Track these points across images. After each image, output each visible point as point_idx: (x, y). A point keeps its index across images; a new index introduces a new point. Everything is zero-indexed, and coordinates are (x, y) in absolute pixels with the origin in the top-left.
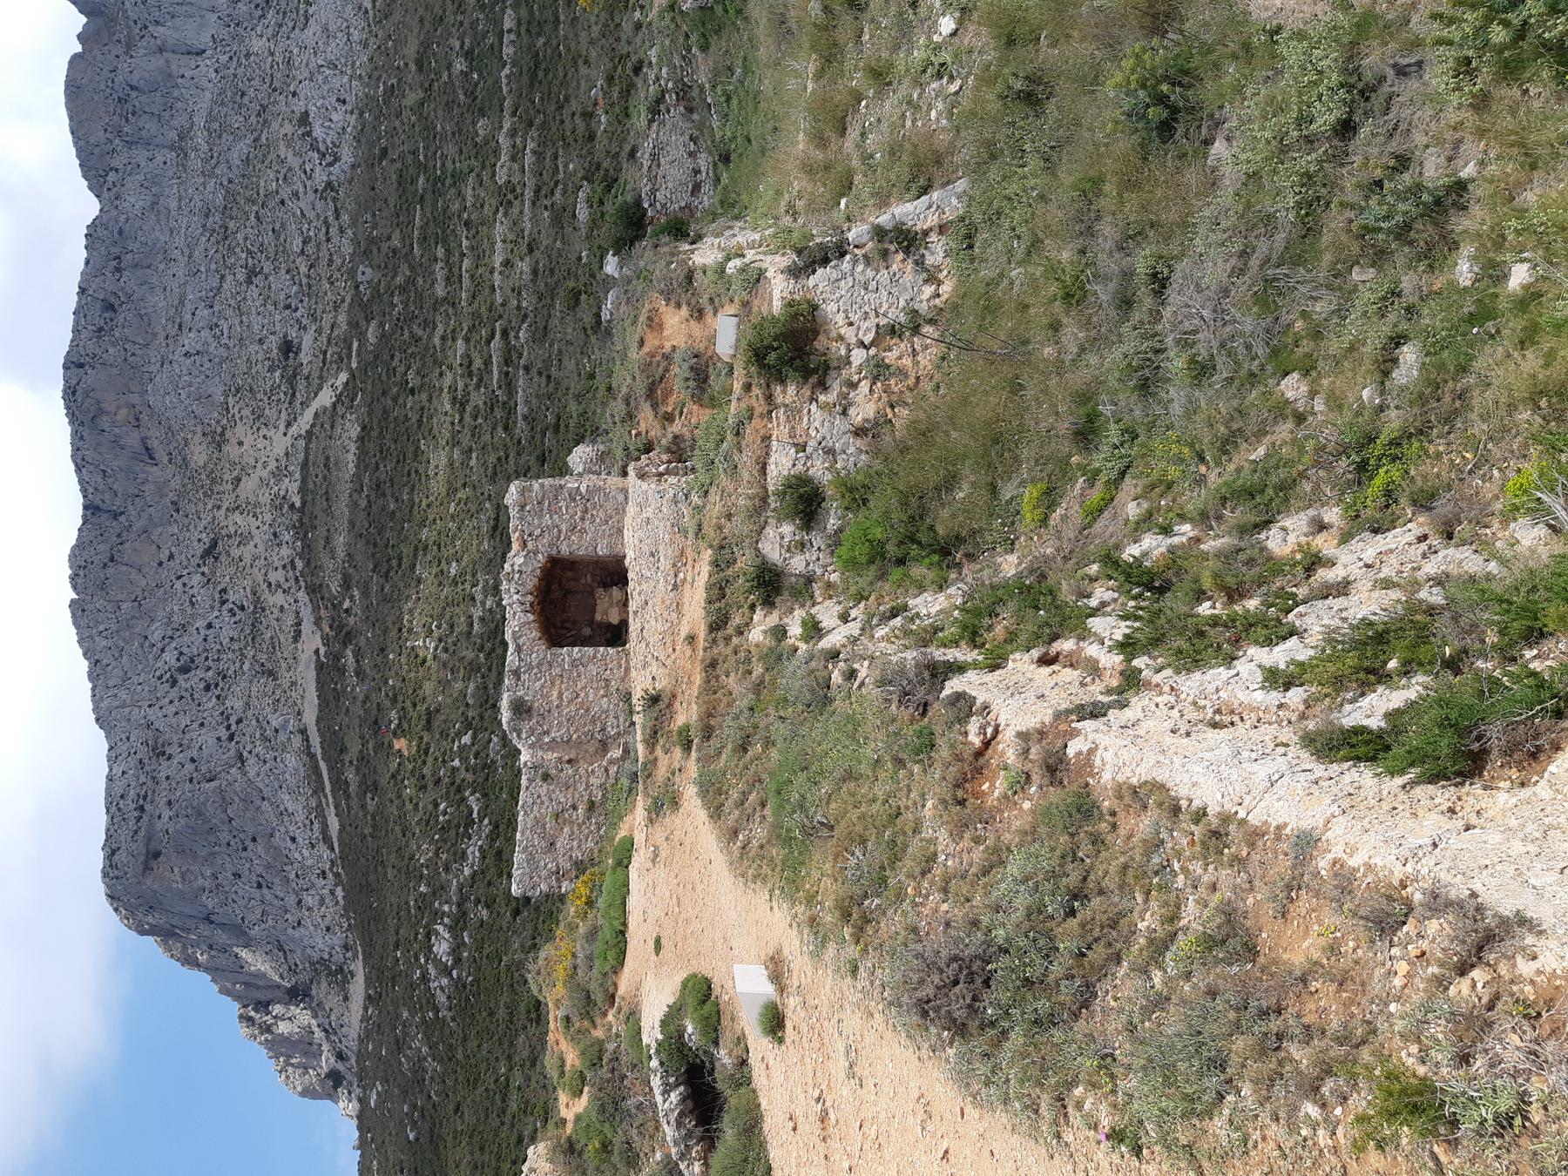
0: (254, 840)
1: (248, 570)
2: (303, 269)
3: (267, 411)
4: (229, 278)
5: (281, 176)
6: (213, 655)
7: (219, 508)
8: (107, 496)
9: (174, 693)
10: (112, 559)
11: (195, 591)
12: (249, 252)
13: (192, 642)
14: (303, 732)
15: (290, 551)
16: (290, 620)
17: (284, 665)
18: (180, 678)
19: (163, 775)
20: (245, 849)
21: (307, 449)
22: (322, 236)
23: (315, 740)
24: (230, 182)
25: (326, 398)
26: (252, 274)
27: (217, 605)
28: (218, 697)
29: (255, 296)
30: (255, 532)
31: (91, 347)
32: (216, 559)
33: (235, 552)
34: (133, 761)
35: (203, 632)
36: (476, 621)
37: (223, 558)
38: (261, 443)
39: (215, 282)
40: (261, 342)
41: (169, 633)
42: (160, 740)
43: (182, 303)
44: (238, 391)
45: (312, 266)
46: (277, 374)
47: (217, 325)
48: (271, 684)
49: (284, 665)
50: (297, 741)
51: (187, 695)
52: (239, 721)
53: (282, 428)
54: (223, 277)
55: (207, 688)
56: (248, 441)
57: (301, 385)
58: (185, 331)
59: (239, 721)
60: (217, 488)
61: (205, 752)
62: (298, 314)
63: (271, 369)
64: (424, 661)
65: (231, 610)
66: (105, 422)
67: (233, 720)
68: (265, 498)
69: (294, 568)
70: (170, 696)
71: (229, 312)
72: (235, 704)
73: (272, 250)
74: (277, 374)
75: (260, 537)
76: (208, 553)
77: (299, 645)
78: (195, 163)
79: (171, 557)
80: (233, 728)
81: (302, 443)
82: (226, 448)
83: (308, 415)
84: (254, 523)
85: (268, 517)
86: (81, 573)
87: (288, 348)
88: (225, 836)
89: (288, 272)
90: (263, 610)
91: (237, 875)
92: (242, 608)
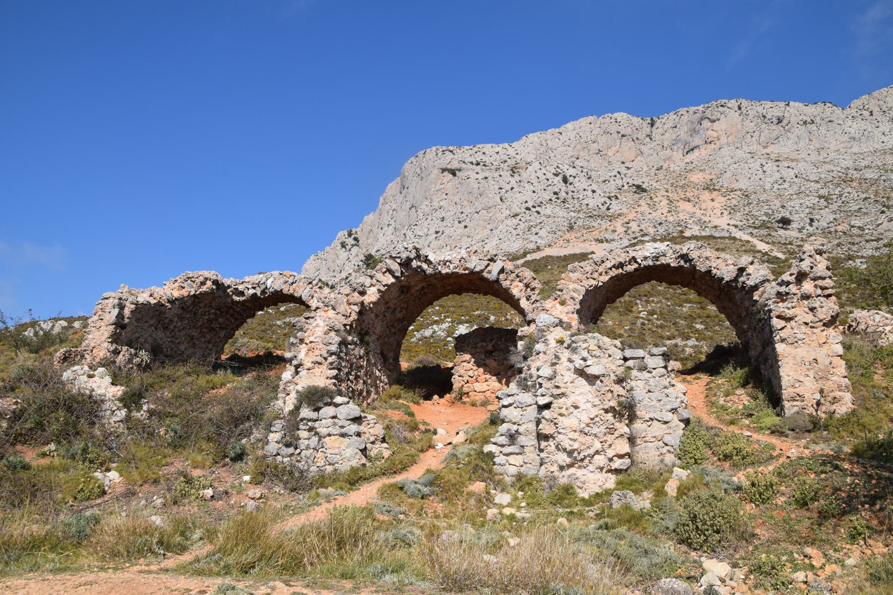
0: (466, 227)
2: (840, 228)
4: (819, 186)
7: (667, 191)
8: (660, 130)
9: (550, 176)
10: (623, 136)
11: (612, 182)
12: (841, 196)
13: (580, 183)
14: (538, 249)
15: (653, 233)
16: (609, 236)
17: (579, 235)
18: (560, 178)
19: (502, 173)
20: (460, 222)
21: (724, 238)
22: (868, 237)
23: (537, 256)
25: (762, 246)
26: (827, 198)
27: (607, 195)
28: (550, 200)
29: (812, 201)
30: (659, 212)
32: (635, 192)
33: (642, 202)
34: (506, 158)
35: (589, 188)
36: (673, 342)
37: (637, 196)
38: (718, 213)
39: (812, 178)
40: (783, 207)
42: (520, 170)
43: (793, 161)
44: (746, 196)
45: (844, 233)
46: (764, 218)
47: (784, 181)
48: (565, 229)
49: (579, 235)
50: (532, 246)
52: (538, 213)
53: (732, 222)
54: (817, 182)
55: (555, 193)
56: (715, 204)
57: (764, 232)
58: (777, 163)
59: (538, 213)
60: (679, 190)
62: (808, 227)
63: (767, 214)
64: (631, 311)
66: (706, 124)
67: (538, 209)
68: (682, 216)
69: (643, 236)
71: (795, 188)
73: (846, 208)
74: (764, 218)
75: (657, 216)
76: (638, 187)
77: (594, 242)
79: (628, 168)
80: (534, 210)
81: (727, 235)
84: (665, 211)
85: (671, 219)
87: (785, 222)
88: (467, 210)
89: (835, 219)
91: (443, 219)
92: (608, 209)
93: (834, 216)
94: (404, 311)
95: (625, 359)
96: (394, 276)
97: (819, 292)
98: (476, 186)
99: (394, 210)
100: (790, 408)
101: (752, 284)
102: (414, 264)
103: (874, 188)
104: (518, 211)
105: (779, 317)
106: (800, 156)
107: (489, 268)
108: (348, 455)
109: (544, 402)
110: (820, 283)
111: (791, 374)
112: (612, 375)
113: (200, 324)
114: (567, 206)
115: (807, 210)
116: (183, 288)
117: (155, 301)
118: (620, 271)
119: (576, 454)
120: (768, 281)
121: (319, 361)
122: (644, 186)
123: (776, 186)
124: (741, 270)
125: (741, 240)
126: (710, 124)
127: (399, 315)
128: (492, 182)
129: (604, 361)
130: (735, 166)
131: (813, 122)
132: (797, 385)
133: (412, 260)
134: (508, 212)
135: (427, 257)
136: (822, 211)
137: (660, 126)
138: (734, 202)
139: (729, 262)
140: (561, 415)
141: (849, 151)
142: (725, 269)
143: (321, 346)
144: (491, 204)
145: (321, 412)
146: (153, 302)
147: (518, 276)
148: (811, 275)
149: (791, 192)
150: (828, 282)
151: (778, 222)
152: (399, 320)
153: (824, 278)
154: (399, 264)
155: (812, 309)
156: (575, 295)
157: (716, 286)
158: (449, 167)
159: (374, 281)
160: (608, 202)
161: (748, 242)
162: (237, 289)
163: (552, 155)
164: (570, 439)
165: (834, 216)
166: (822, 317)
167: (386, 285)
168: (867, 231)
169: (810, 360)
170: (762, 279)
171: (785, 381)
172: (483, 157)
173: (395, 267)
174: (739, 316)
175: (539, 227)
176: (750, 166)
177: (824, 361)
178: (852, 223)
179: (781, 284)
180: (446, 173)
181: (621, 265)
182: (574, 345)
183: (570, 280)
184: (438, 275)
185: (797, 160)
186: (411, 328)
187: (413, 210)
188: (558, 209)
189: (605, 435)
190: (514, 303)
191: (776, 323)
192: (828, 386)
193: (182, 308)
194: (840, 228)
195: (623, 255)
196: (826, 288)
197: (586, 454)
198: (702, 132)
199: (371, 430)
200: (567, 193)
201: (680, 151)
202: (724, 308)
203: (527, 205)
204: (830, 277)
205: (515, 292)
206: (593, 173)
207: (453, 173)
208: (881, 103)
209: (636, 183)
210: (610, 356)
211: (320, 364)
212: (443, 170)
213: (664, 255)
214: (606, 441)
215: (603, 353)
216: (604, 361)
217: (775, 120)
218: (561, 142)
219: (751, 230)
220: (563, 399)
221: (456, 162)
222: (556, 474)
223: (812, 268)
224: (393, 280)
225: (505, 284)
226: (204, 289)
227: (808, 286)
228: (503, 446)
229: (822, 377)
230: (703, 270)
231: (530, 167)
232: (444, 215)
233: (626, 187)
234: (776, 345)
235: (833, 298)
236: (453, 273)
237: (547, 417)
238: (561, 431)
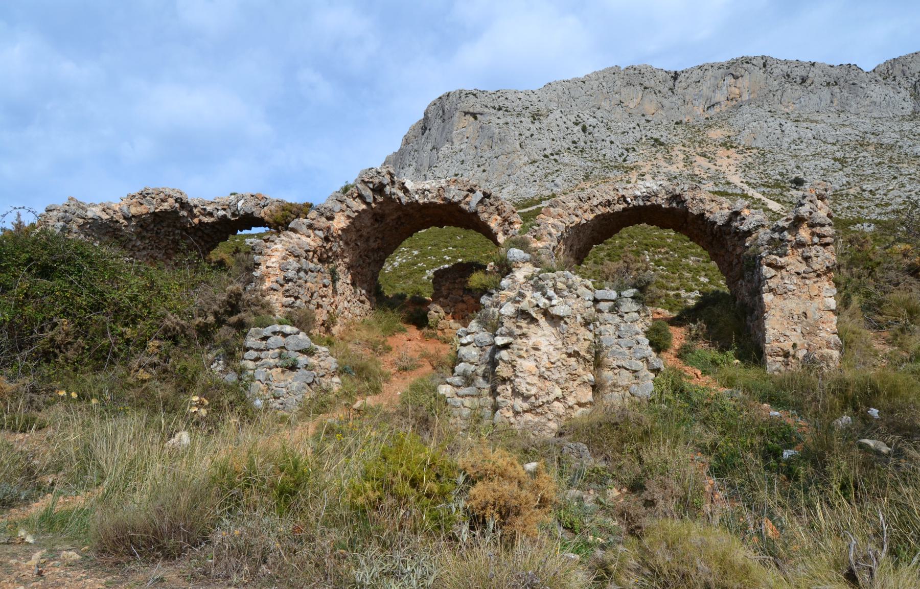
1: (650, 163)
2: (852, 191)
3: (753, 172)
4: (835, 148)
5: (912, 176)
6: (594, 145)
9: (570, 124)
10: (645, 88)
11: (631, 134)
12: (856, 159)
13: (600, 133)
18: (579, 128)
19: (523, 119)
20: (479, 166)
24: (900, 147)
26: (843, 161)
27: (625, 146)
28: (569, 149)
29: (828, 163)
31: (777, 72)
33: (659, 155)
34: (527, 104)
35: (608, 139)
37: (654, 149)
39: (830, 140)
40: (798, 167)
41: (605, 121)
42: (541, 118)
43: (812, 122)
46: (779, 177)
50: (547, 193)
51: (569, 131)
52: (555, 160)
54: (834, 144)
55: (574, 142)
56: (731, 161)
57: (777, 191)
58: (796, 124)
61: (537, 142)
63: (781, 174)
65: (623, 154)
66: (729, 80)
70: (568, 122)
71: (812, 149)
72: (566, 158)
73: (860, 172)
74: (779, 177)
76: (656, 140)
78: (907, 126)
79: (648, 121)
80: (552, 157)
81: (739, 192)
82: (724, 148)
83: (758, 195)
86: (636, 72)
87: (798, 182)
88: (487, 154)
90: (626, 172)
91: (462, 162)
92: (625, 160)
93: (847, 179)
94: (379, 241)
95: (596, 301)
96: (365, 202)
97: (816, 240)
98: (497, 131)
99: (416, 151)
100: (774, 364)
101: (745, 229)
102: (388, 189)
103: (889, 154)
104: (537, 157)
105: (769, 265)
106: (820, 118)
107: (467, 199)
108: (294, 388)
109: (503, 342)
110: (818, 230)
111: (777, 327)
112: (579, 317)
113: (164, 244)
114: (585, 155)
115: (822, 172)
116: (141, 204)
117: (108, 217)
118: (608, 209)
119: (533, 399)
120: (763, 226)
121: (275, 287)
122: (662, 140)
123: (793, 147)
124: (736, 214)
125: (753, 198)
126: (733, 80)
127: (373, 245)
128: (513, 128)
129: (571, 301)
130: (754, 124)
131: (836, 84)
132: (782, 339)
133: (385, 186)
134: (526, 159)
135: (403, 184)
136: (836, 174)
137: (683, 80)
138: (750, 160)
139: (724, 205)
140: (520, 357)
141: (870, 115)
142: (718, 213)
143: (278, 272)
144: (510, 150)
145: (269, 341)
146: (105, 217)
147: (497, 209)
148: (810, 221)
149: (808, 153)
150: (828, 230)
151: (791, 182)
152: (373, 250)
153: (823, 225)
154: (372, 190)
155: (807, 259)
156: (553, 231)
157: (708, 230)
158: (471, 110)
159: (344, 207)
160: (626, 153)
161: (760, 200)
162: (205, 209)
163: (574, 104)
164: (528, 383)
165: (847, 179)
166: (816, 266)
167: (357, 211)
168: (878, 196)
169: (801, 313)
170: (757, 224)
171: (770, 334)
172: (506, 102)
173: (368, 194)
174: (731, 264)
175: (556, 175)
176: (770, 124)
177: (813, 314)
178: (864, 187)
179: (774, 230)
180: (468, 116)
181: (609, 203)
182: (541, 283)
183: (550, 215)
184: (414, 205)
185: (816, 122)
186: (447, 266)
187: (434, 151)
188: (575, 158)
189: (566, 381)
190: (491, 235)
191: (767, 271)
192: (816, 341)
193: (141, 226)
194: (852, 191)
195: (612, 193)
196: (825, 236)
197: (545, 400)
198: (725, 88)
199: (322, 364)
200: (586, 143)
201: (701, 107)
202: (716, 255)
203: (546, 152)
204: (830, 225)
205: (493, 225)
206: (613, 124)
207: (474, 116)
208: (905, 68)
209: (655, 136)
210: (578, 297)
211: (275, 290)
212: (466, 113)
213: (656, 195)
214: (567, 388)
215: (574, 294)
216: (571, 301)
217: (799, 80)
218: (583, 92)
219: (763, 189)
220: (524, 340)
221: (478, 106)
222: (512, 420)
223: (811, 213)
224: (364, 207)
225: (484, 216)
226: (166, 206)
227: (804, 234)
228: (458, 387)
229: (809, 333)
230: (695, 213)
231: (551, 115)
232: (463, 158)
233: (644, 140)
234: (764, 296)
235: (831, 246)
236: (431, 203)
237: (506, 358)
238: (519, 374)
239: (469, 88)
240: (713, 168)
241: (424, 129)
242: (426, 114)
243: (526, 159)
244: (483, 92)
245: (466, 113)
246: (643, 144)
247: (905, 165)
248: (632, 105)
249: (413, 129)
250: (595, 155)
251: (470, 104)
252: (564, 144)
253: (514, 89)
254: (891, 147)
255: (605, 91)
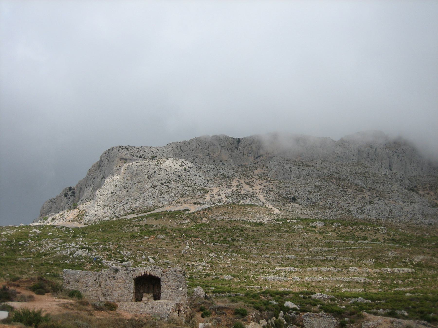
2: (321, 203)
10: (222, 147)
20: (125, 188)
27: (207, 178)
28: (176, 179)
52: (167, 186)
55: (179, 176)
58: (298, 167)
72: (173, 185)
79: (224, 164)
80: (165, 184)
88: (129, 182)
104: (157, 184)
128: (145, 168)
130: (277, 167)
138: (272, 186)
144: (142, 180)
158: (124, 157)
194: (321, 203)
200: (186, 177)
201: (253, 157)
212: (121, 159)
221: (128, 155)
232: (117, 184)
239: (125, 145)
240: (252, 191)
241: (100, 166)
242: (101, 158)
243: (151, 184)
244: (132, 147)
245: (121, 159)
246: (218, 177)
247: (349, 190)
248: (215, 156)
249: (94, 166)
250: (190, 184)
251: (123, 154)
252: (173, 177)
253: (150, 146)
254: (344, 180)
255: (200, 148)
